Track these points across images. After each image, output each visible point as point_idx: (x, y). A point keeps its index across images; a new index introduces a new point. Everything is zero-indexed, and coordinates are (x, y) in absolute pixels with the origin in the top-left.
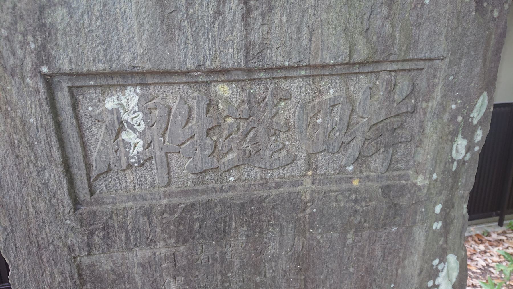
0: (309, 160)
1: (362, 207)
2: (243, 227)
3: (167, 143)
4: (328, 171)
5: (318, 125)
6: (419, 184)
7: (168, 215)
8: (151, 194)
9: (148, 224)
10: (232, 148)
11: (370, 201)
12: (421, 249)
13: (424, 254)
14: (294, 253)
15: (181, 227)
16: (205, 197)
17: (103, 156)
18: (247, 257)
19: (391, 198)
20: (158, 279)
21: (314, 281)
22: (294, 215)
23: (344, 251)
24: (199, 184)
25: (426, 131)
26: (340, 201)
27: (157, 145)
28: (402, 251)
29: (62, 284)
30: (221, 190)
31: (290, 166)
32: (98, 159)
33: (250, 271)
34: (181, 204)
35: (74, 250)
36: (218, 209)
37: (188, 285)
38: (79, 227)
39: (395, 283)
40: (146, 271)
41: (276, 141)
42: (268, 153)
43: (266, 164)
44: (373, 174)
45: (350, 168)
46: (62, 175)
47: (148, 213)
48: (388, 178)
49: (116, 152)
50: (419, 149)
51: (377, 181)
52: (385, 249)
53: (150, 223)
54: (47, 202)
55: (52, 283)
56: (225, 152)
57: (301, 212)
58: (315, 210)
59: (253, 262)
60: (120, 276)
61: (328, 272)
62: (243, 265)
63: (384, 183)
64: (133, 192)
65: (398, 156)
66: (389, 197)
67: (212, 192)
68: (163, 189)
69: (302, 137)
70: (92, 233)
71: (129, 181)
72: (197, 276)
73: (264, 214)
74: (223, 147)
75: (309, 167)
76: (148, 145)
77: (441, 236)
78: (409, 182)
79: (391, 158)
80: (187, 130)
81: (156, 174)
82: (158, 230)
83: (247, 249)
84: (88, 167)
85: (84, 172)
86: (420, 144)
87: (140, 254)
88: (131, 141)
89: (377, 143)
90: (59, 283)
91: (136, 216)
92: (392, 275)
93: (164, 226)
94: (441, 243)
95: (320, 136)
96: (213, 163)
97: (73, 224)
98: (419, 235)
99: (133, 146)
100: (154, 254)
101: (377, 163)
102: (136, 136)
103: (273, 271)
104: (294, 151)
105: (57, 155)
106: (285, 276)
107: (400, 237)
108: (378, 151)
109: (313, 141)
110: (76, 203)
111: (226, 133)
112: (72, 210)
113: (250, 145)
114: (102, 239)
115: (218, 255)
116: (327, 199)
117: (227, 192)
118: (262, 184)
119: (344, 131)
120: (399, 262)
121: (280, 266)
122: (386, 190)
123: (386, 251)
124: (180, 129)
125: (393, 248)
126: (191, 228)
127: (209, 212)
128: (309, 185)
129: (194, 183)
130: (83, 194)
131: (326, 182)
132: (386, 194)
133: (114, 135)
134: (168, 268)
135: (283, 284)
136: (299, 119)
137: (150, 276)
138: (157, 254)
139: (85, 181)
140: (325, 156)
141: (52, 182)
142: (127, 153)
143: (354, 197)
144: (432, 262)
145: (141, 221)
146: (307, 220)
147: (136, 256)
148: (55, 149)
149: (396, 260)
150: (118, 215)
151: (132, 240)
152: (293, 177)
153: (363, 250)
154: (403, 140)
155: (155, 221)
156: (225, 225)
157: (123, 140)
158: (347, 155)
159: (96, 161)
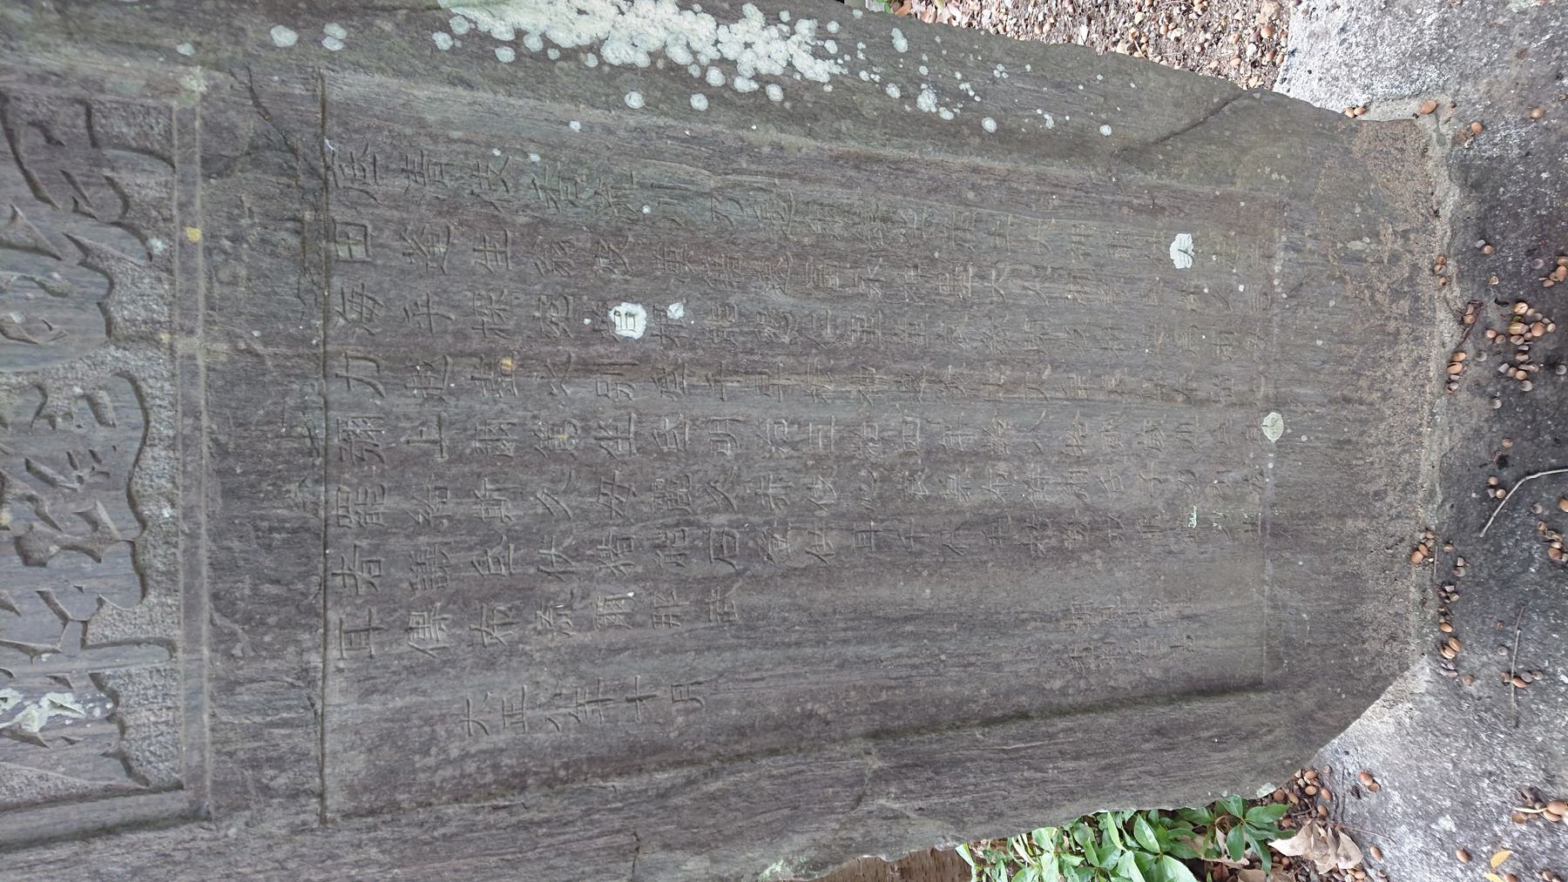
0: (128, 338)
1: (252, 226)
2: (288, 491)
3: (58, 647)
4: (162, 297)
5: (28, 321)
6: (203, 89)
7: (239, 646)
8: (187, 677)
9: (255, 686)
10: (79, 514)
11: (240, 206)
12: (394, 83)
13: (407, 76)
14: (380, 378)
15: (272, 620)
16: (205, 570)
17: (83, 767)
18: (377, 480)
19: (238, 154)
20: (405, 662)
21: (461, 335)
22: (268, 378)
23: (384, 266)
24: (175, 583)
25: (56, 69)
26: (235, 276)
27: (60, 667)
28: (397, 127)
29: (385, 847)
30: (193, 536)
31: (142, 384)
32: (88, 775)
33: (415, 474)
34: (212, 621)
35: (304, 823)
36: (236, 544)
37: (433, 603)
38: (247, 813)
39: (490, 146)
40: (382, 687)
41: (68, 416)
42: (102, 433)
43: (130, 438)
44: (176, 194)
45: (158, 245)
46: (116, 841)
47: (228, 686)
48: (187, 160)
49: (71, 742)
50: (108, 86)
51: (194, 184)
52: (387, 169)
53: (252, 681)
54: (178, 869)
55: (381, 865)
56: (89, 527)
57: (263, 363)
58: (256, 334)
59: (395, 468)
60: (386, 738)
61: (439, 303)
62: (401, 489)
63: (198, 169)
64: (181, 712)
65: (129, 132)
66: (235, 159)
67: (194, 554)
68: (180, 654)
69: (60, 358)
70: (266, 790)
71: (152, 719)
72: (412, 585)
73: (259, 446)
74: (79, 532)
75: (150, 339)
76: (62, 683)
77: (370, 25)
78: (198, 109)
79: (134, 150)
80: (24, 607)
81: (141, 666)
82: (271, 665)
83: (355, 481)
84: (109, 793)
85: (119, 802)
86: (94, 82)
87: (334, 698)
88: (46, 716)
89: (87, 184)
90: (383, 852)
91: (232, 707)
92: (466, 154)
93: (264, 653)
94: (388, 27)
95: (60, 315)
96: (118, 554)
97: (241, 823)
98: (350, 86)
99: (58, 712)
100: (340, 671)
101: (146, 183)
102: (35, 706)
103: (423, 424)
104: (105, 374)
105: (63, 851)
106: (441, 399)
107: (356, 131)
108: (111, 182)
109: (72, 332)
110: (193, 816)
111: (38, 526)
112: (206, 824)
113: (75, 473)
114: (284, 771)
115: (364, 543)
116: (228, 303)
117: (198, 524)
118: (186, 446)
119: (49, 261)
120: (430, 135)
121: (412, 410)
122: (215, 166)
123: (393, 166)
124: (20, 620)
125: (388, 149)
126: (277, 601)
127: (241, 563)
128: (195, 341)
129: (170, 592)
130: (176, 803)
131: (188, 303)
132: (227, 167)
133: (28, 746)
134: (381, 644)
135: (461, 403)
136: (10, 364)
137: (396, 678)
138: (341, 665)
139: (142, 799)
140: (120, 302)
141: (129, 859)
142: (77, 722)
143: (227, 244)
144: (439, 51)
145: (246, 698)
146: (283, 350)
147: (339, 705)
148: (48, 854)
149: (425, 143)
150: (228, 741)
151: (293, 715)
152: (173, 375)
153: (387, 221)
154: (81, 122)
155: (247, 671)
156: (278, 530)
157: (42, 730)
158: (117, 253)
159: (93, 779)
